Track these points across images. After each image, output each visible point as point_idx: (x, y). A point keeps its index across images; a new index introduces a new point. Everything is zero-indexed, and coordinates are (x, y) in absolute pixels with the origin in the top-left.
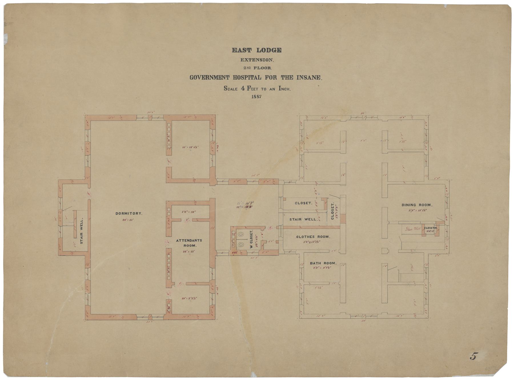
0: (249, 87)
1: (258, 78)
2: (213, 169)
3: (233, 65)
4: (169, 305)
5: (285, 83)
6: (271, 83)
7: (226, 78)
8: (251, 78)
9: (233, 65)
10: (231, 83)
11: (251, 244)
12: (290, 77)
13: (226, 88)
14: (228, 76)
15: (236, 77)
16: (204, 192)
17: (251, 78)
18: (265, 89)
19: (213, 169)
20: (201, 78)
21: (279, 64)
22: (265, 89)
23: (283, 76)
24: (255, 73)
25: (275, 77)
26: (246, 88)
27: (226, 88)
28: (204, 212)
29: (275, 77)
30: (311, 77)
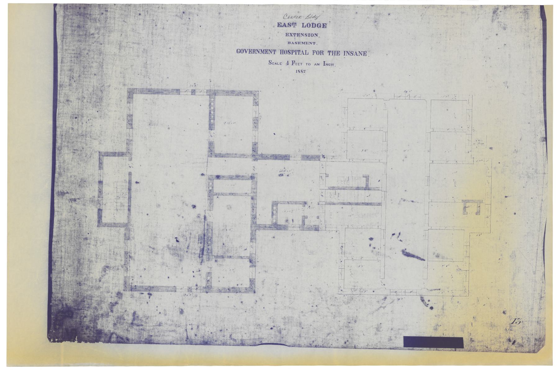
0: (293, 62)
1: (306, 53)
2: (367, 185)
3: (280, 39)
4: (209, 278)
5: (329, 58)
6: (319, 59)
7: (273, 53)
8: (297, 53)
9: (280, 39)
10: (277, 57)
11: (429, 306)
12: (337, 53)
13: (270, 62)
14: (275, 51)
15: (282, 52)
16: (246, 166)
17: (297, 53)
18: (309, 64)
19: (367, 185)
20: (248, 52)
21: (327, 39)
22: (309, 64)
23: (329, 52)
24: (302, 47)
25: (321, 53)
26: (290, 63)
27: (270, 62)
28: (246, 186)
29: (321, 53)
30: (358, 53)
